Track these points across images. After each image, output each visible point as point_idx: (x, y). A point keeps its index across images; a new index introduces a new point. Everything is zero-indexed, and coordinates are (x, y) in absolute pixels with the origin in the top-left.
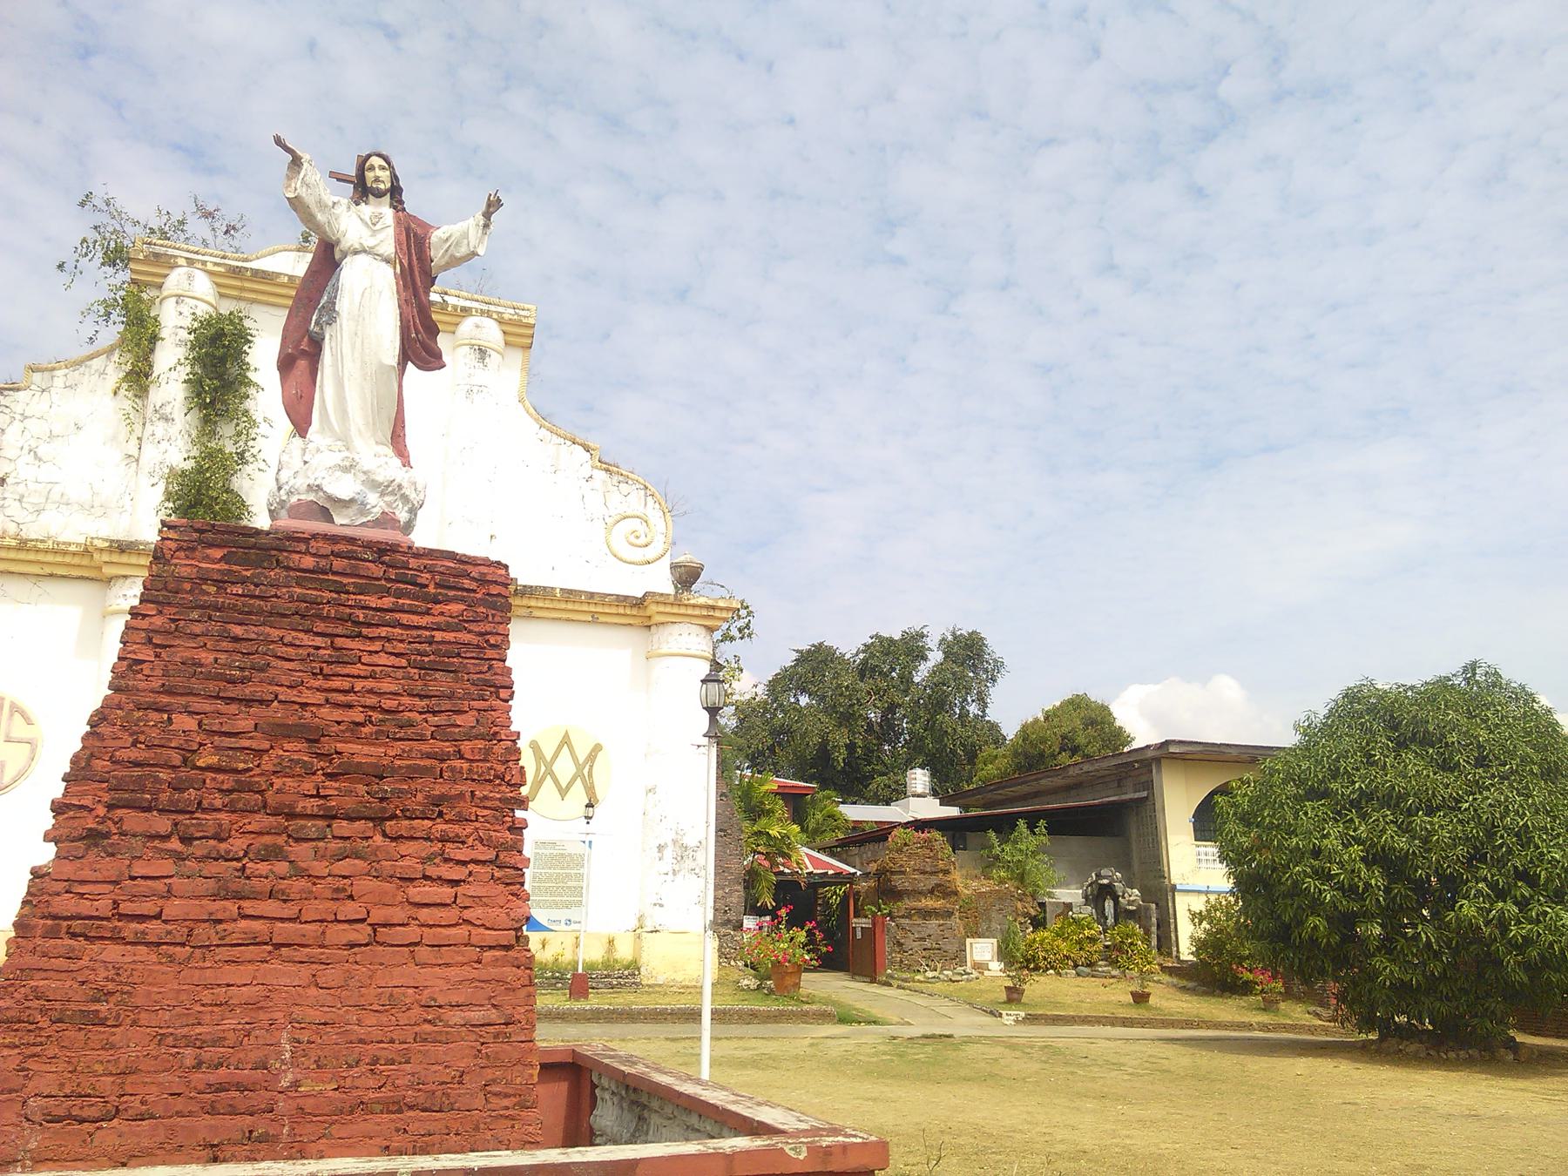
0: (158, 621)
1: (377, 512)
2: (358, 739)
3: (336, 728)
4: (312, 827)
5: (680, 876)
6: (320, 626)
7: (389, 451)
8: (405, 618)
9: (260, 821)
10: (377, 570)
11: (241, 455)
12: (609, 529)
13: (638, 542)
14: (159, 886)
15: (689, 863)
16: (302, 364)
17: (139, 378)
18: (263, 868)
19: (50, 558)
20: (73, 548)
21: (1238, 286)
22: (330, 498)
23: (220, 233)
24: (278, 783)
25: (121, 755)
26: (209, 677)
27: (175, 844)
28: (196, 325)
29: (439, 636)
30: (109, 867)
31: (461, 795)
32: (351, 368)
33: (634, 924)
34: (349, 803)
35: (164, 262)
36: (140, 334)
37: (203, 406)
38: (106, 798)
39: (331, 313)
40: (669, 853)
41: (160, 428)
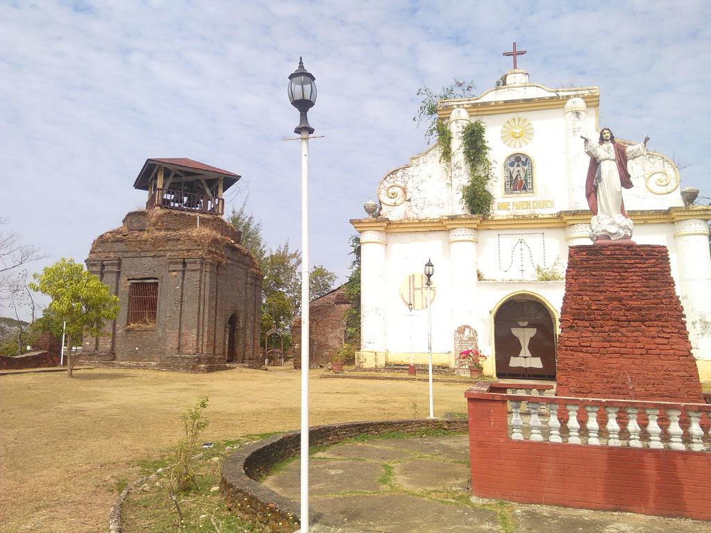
0: (574, 273)
1: (623, 234)
2: (632, 300)
3: (625, 298)
4: (625, 324)
6: (616, 270)
7: (621, 215)
8: (639, 265)
9: (611, 323)
10: (628, 253)
11: (487, 176)
12: (647, 180)
13: (663, 184)
14: (589, 339)
16: (593, 194)
17: (447, 154)
18: (614, 334)
19: (429, 225)
20: (436, 221)
21: (479, 276)
22: (610, 233)
24: (613, 312)
25: (572, 307)
26: (589, 286)
27: (591, 329)
28: (464, 130)
29: (649, 269)
31: (665, 314)
32: (609, 195)
34: (634, 317)
35: (449, 108)
36: (445, 136)
37: (470, 161)
38: (572, 318)
39: (600, 178)
41: (457, 172)
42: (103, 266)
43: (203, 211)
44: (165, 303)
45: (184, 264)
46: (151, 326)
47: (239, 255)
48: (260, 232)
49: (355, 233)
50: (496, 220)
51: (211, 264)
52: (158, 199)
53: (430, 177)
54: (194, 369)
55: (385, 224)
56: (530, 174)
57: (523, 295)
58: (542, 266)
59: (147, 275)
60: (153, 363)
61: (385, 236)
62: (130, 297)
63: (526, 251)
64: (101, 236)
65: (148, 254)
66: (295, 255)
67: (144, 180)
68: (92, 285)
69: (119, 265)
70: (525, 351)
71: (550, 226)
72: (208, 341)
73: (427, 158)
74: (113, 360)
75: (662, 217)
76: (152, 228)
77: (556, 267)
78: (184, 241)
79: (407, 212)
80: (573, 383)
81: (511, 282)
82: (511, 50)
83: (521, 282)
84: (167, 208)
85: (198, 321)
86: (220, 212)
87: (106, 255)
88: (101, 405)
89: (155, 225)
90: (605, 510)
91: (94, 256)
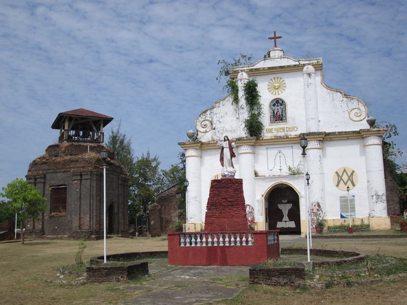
5: (378, 203)
12: (349, 113)
15: (380, 200)
17: (236, 100)
21: (256, 174)
23: (247, 60)
30: (211, 211)
33: (368, 216)
35: (237, 72)
36: (234, 88)
40: (374, 197)
41: (242, 111)
42: (36, 179)
43: (93, 141)
44: (71, 200)
45: (81, 176)
46: (63, 214)
47: (114, 167)
48: (132, 145)
49: (182, 150)
50: (265, 140)
51: (96, 175)
52: (65, 136)
53: (226, 114)
54: (89, 238)
55: (199, 145)
56: (284, 110)
57: (282, 184)
58: (291, 166)
59: (60, 183)
60: (66, 236)
61: (200, 153)
62: (51, 197)
63: (283, 158)
64: (34, 161)
65: (60, 170)
66: (155, 160)
67: (57, 125)
68: (34, 192)
69: (45, 178)
70: (286, 218)
71: (295, 142)
72: (96, 221)
73: (224, 102)
74: (43, 235)
75: (356, 135)
76: (62, 155)
77: (299, 167)
78: (81, 162)
79: (213, 137)
80: (209, 228)
81: (274, 177)
82: (273, 36)
83: (279, 177)
84: (70, 141)
85: (90, 209)
86: (102, 141)
87: (37, 172)
88: (43, 254)
89: (64, 153)
90: (206, 265)
91: (30, 173)
